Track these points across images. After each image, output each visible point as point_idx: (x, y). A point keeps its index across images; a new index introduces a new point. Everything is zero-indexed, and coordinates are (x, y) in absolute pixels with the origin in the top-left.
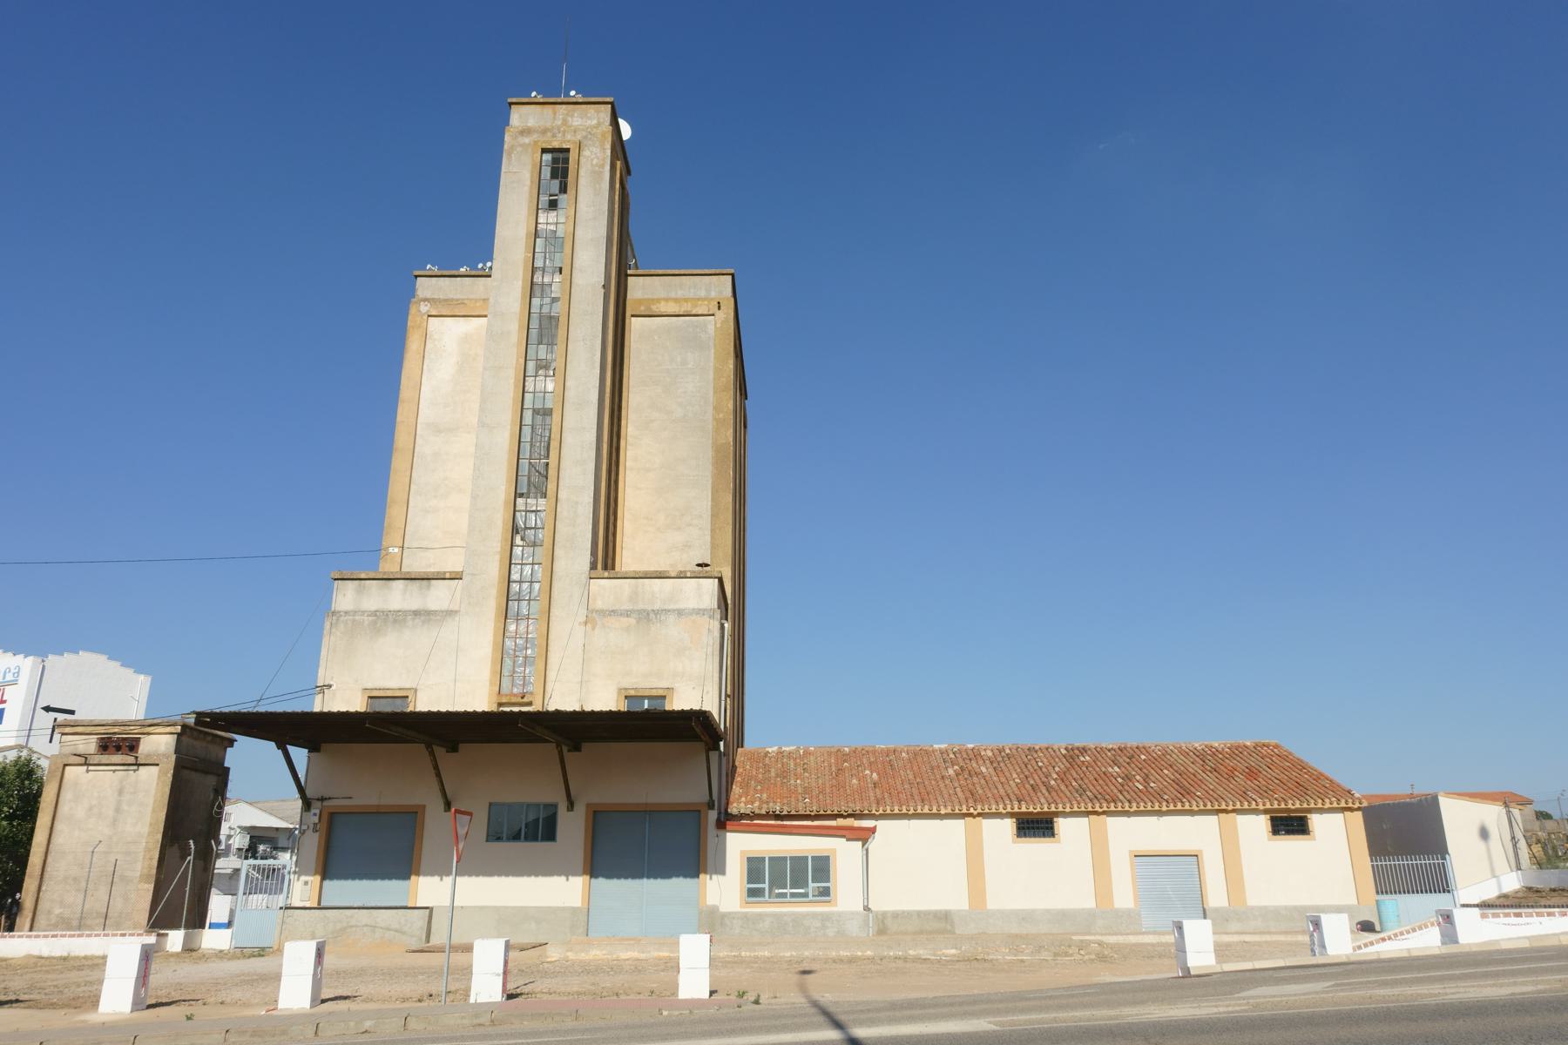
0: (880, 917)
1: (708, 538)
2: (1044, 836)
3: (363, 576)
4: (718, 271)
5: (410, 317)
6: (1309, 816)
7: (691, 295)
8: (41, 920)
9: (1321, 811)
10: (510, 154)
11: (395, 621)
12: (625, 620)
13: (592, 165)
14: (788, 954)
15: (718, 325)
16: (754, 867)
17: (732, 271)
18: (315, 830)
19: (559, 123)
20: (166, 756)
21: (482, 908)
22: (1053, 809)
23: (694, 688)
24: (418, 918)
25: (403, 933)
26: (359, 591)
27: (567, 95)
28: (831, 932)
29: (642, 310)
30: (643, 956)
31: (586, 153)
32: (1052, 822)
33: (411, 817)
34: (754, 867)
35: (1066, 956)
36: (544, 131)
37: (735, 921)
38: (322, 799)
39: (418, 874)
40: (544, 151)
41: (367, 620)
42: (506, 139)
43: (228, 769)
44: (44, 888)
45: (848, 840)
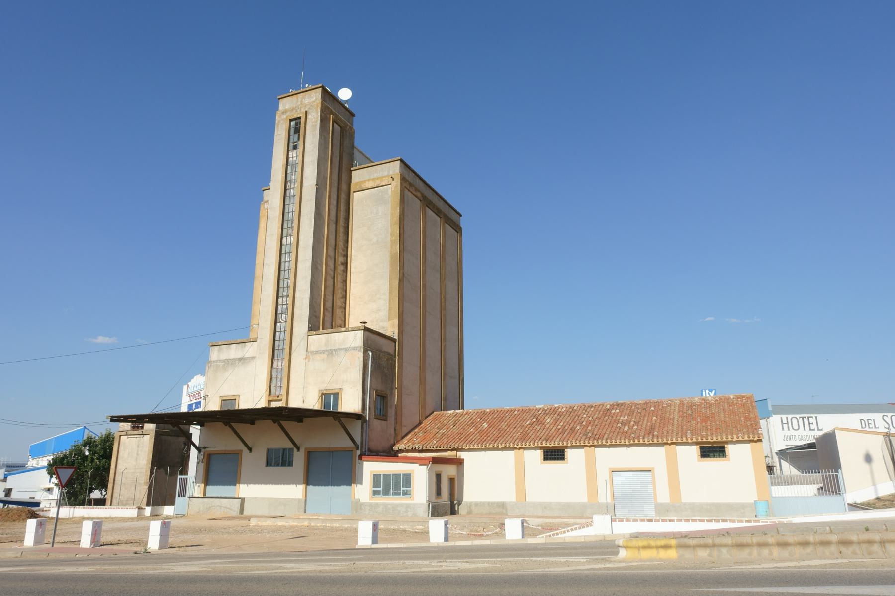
0: (468, 505)
1: (388, 305)
2: (720, 457)
3: (220, 344)
4: (393, 160)
5: (261, 211)
6: (726, 446)
7: (381, 175)
8: (114, 501)
9: (572, 447)
10: (278, 125)
11: (232, 364)
12: (322, 355)
13: (312, 122)
14: (346, 526)
15: (393, 189)
16: (376, 478)
17: (399, 158)
18: (202, 462)
19: (299, 103)
20: (152, 430)
21: (263, 498)
22: (565, 444)
23: (351, 388)
24: (237, 502)
25: (231, 509)
26: (219, 351)
27: (304, 87)
28: (410, 514)
29: (358, 188)
30: (287, 524)
31: (309, 117)
32: (563, 452)
33: (237, 455)
34: (376, 478)
35: (476, 532)
36: (292, 110)
37: (367, 507)
38: (205, 448)
39: (239, 483)
40: (291, 120)
41: (221, 364)
42: (277, 118)
43: (192, 434)
44: (115, 488)
45: (420, 465)
